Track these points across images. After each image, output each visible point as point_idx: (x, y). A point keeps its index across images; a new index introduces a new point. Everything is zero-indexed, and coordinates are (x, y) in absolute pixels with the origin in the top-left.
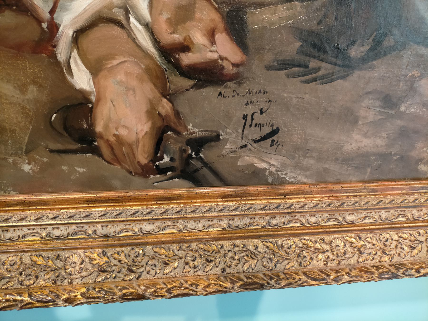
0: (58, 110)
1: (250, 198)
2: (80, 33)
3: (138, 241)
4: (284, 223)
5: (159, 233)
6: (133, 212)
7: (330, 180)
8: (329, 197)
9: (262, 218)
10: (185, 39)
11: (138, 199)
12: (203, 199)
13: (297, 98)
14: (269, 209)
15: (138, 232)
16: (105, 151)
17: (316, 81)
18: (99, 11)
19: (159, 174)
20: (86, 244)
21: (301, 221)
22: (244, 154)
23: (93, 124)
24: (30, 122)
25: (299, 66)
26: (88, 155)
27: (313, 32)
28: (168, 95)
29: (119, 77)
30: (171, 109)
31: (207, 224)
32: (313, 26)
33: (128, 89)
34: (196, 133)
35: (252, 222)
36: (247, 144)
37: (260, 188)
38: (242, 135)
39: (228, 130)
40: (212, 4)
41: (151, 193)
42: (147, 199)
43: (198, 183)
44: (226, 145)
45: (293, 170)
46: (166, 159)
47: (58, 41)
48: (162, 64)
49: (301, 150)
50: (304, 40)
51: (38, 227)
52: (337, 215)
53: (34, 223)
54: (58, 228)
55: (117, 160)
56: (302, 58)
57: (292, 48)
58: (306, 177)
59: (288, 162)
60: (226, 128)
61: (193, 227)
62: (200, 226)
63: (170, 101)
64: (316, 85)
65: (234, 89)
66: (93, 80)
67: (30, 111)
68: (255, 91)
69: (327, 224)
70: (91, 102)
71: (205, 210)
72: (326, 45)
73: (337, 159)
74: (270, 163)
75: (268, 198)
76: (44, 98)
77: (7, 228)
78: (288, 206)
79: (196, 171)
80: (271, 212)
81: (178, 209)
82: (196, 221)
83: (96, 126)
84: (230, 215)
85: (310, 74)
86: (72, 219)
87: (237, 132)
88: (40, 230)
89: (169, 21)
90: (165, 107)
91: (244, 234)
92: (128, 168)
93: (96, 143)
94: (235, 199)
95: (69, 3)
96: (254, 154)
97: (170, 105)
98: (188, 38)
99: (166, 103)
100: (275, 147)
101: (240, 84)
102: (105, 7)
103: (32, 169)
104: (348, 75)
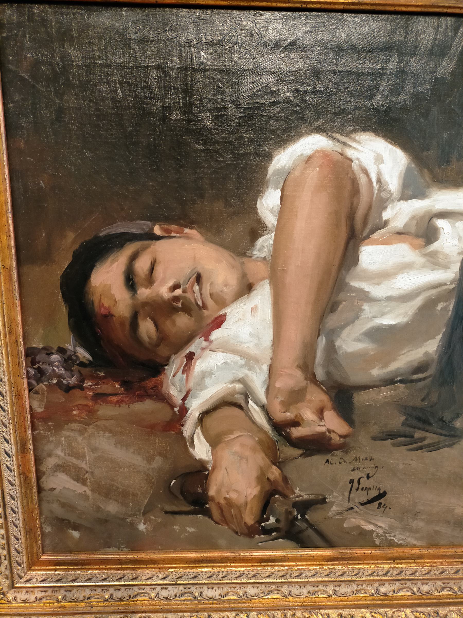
0: (177, 477)
1: (357, 562)
2: (205, 414)
3: (243, 605)
4: (394, 592)
5: (263, 598)
6: (238, 574)
7: (442, 542)
8: (442, 562)
9: (370, 585)
10: (296, 417)
11: (243, 560)
12: (308, 562)
13: (404, 464)
14: (378, 575)
15: (242, 596)
16: (215, 513)
17: (422, 449)
18: (224, 397)
19: (264, 534)
20: (192, 606)
21: (412, 590)
22: (351, 516)
23: (207, 489)
24: (151, 488)
25: (405, 436)
26: (199, 516)
27: (417, 408)
28: (276, 461)
29: (235, 448)
30: (279, 474)
31: (312, 589)
32: (417, 402)
33: (241, 458)
34: (303, 496)
35: (359, 589)
36: (353, 506)
37: (368, 551)
38: (349, 498)
39: (335, 494)
40: (322, 389)
41: (256, 554)
42: (252, 560)
43: (303, 544)
44: (332, 507)
45: (402, 532)
46: (272, 520)
47: (185, 421)
48: (274, 437)
49: (408, 513)
50: (408, 414)
51: (147, 587)
52: (451, 584)
53: (144, 583)
54: (166, 589)
55: (225, 520)
56: (408, 430)
57: (397, 421)
58: (416, 539)
59: (396, 524)
60: (333, 492)
61: (297, 593)
62: (305, 591)
63: (279, 467)
64: (423, 452)
65: (341, 457)
66: (212, 451)
67: (153, 479)
68: (361, 458)
69: (441, 594)
70: (207, 470)
71: (310, 575)
72: (430, 418)
73: (448, 522)
74: (377, 525)
75: (376, 562)
76: (167, 466)
77: (119, 587)
78: (397, 572)
79: (301, 531)
80: (380, 578)
81: (283, 573)
82: (301, 587)
83: (210, 490)
84: (335, 581)
85: (416, 443)
86: (180, 579)
87: (344, 495)
88: (149, 590)
89: (282, 403)
90: (275, 473)
91: (351, 603)
92: (235, 528)
93: (207, 506)
94: (341, 562)
95: (199, 392)
96: (361, 516)
97: (279, 471)
98: (299, 416)
99: (275, 470)
100: (382, 509)
101: (346, 452)
102: (228, 394)
103: (146, 528)
104: (454, 444)
